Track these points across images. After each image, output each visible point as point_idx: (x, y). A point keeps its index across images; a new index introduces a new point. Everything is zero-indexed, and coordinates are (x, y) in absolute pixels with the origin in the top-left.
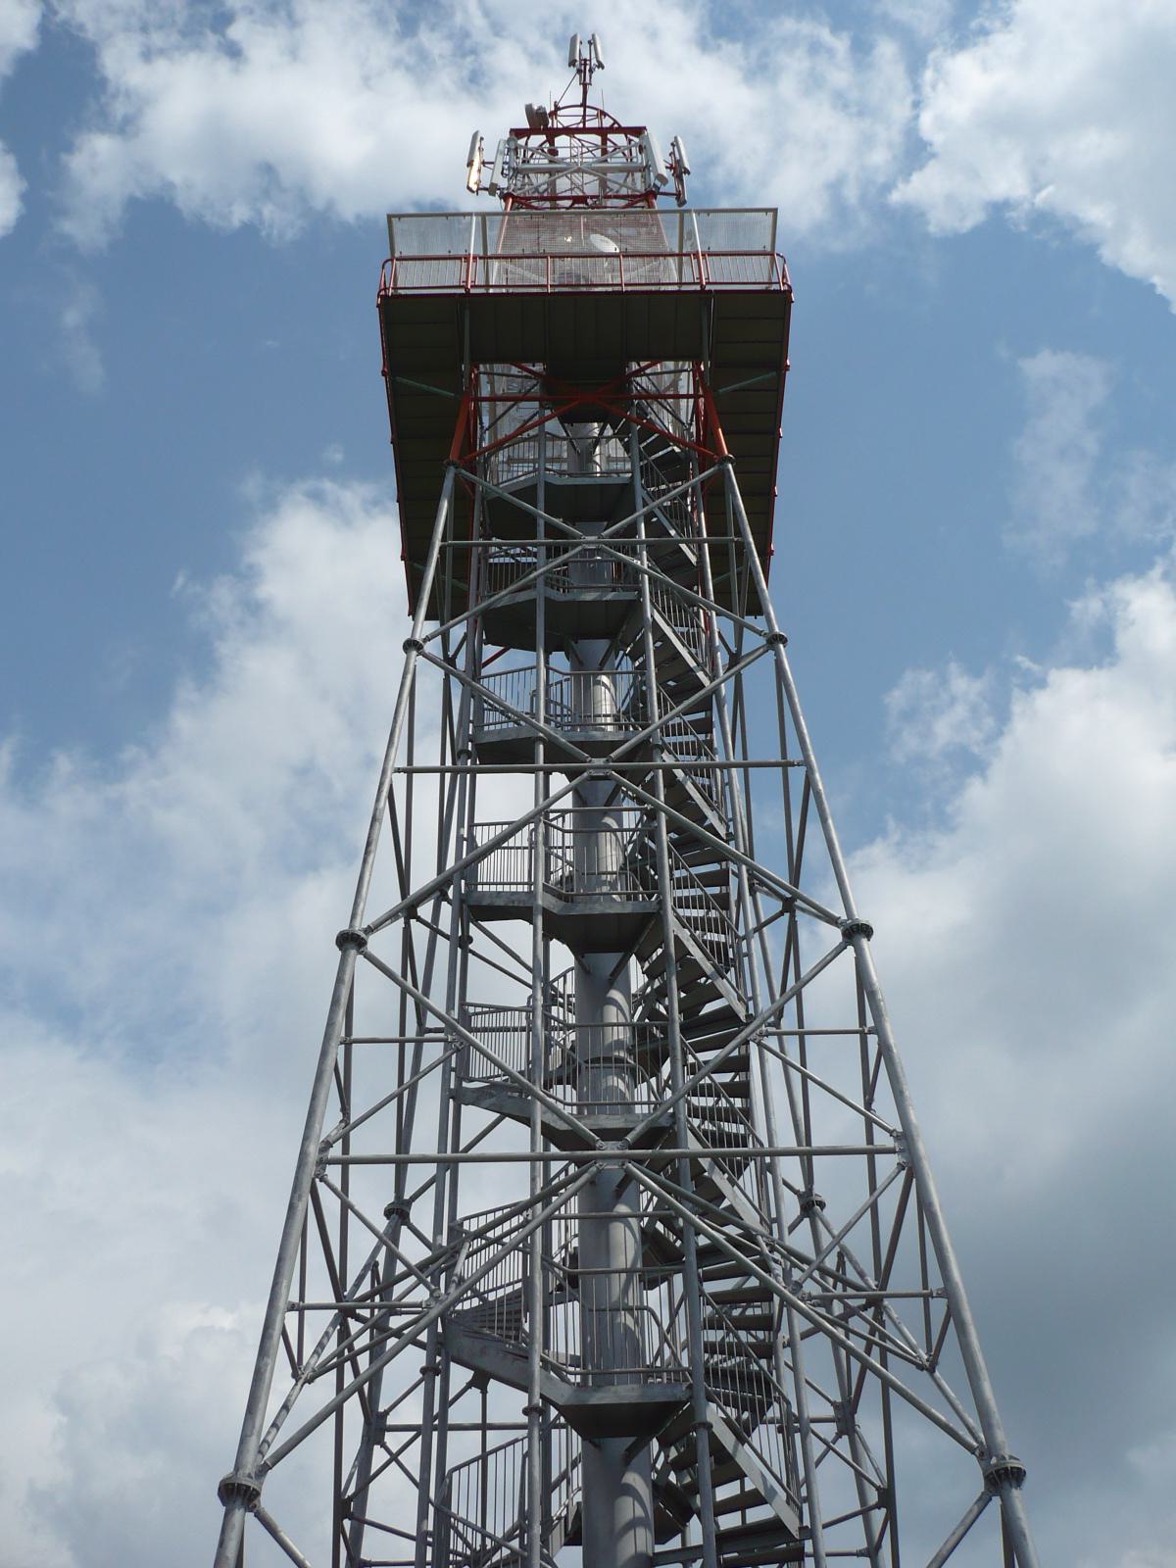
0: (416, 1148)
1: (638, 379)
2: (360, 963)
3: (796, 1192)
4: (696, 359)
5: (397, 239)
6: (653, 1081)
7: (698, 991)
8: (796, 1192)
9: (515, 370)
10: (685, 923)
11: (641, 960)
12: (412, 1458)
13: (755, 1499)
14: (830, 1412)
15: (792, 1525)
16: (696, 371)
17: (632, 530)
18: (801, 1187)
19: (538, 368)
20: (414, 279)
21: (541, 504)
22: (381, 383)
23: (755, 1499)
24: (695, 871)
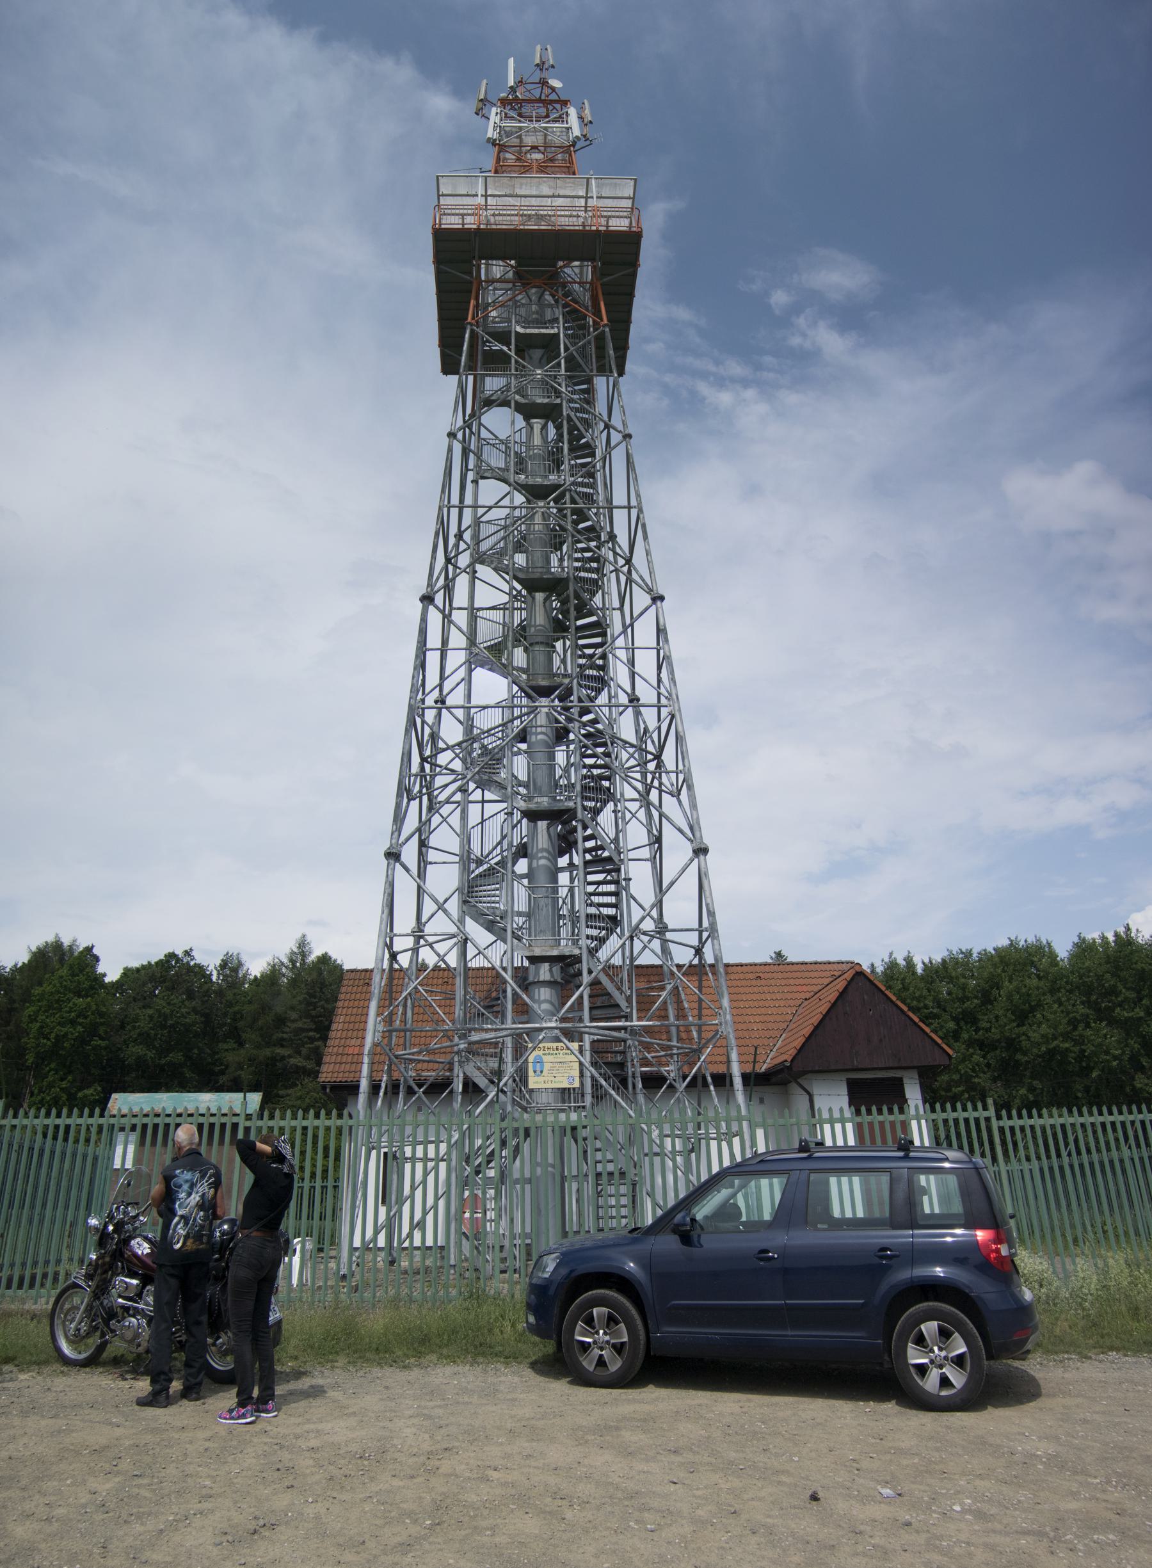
0: (452, 503)
1: (566, 270)
2: (431, 608)
3: (627, 693)
4: (593, 260)
5: (441, 186)
6: (559, 553)
7: (575, 436)
8: (627, 693)
9: (501, 263)
10: (572, 409)
11: (554, 422)
12: (455, 820)
13: (602, 848)
14: (636, 796)
15: (616, 859)
16: (594, 268)
17: (559, 364)
18: (629, 690)
19: (513, 262)
20: (452, 222)
21: (513, 347)
22: (438, 350)
23: (602, 848)
24: (577, 388)
